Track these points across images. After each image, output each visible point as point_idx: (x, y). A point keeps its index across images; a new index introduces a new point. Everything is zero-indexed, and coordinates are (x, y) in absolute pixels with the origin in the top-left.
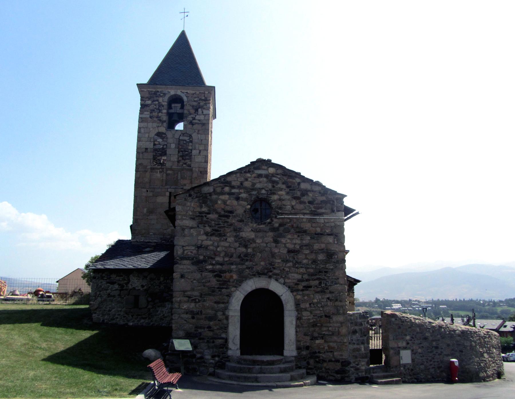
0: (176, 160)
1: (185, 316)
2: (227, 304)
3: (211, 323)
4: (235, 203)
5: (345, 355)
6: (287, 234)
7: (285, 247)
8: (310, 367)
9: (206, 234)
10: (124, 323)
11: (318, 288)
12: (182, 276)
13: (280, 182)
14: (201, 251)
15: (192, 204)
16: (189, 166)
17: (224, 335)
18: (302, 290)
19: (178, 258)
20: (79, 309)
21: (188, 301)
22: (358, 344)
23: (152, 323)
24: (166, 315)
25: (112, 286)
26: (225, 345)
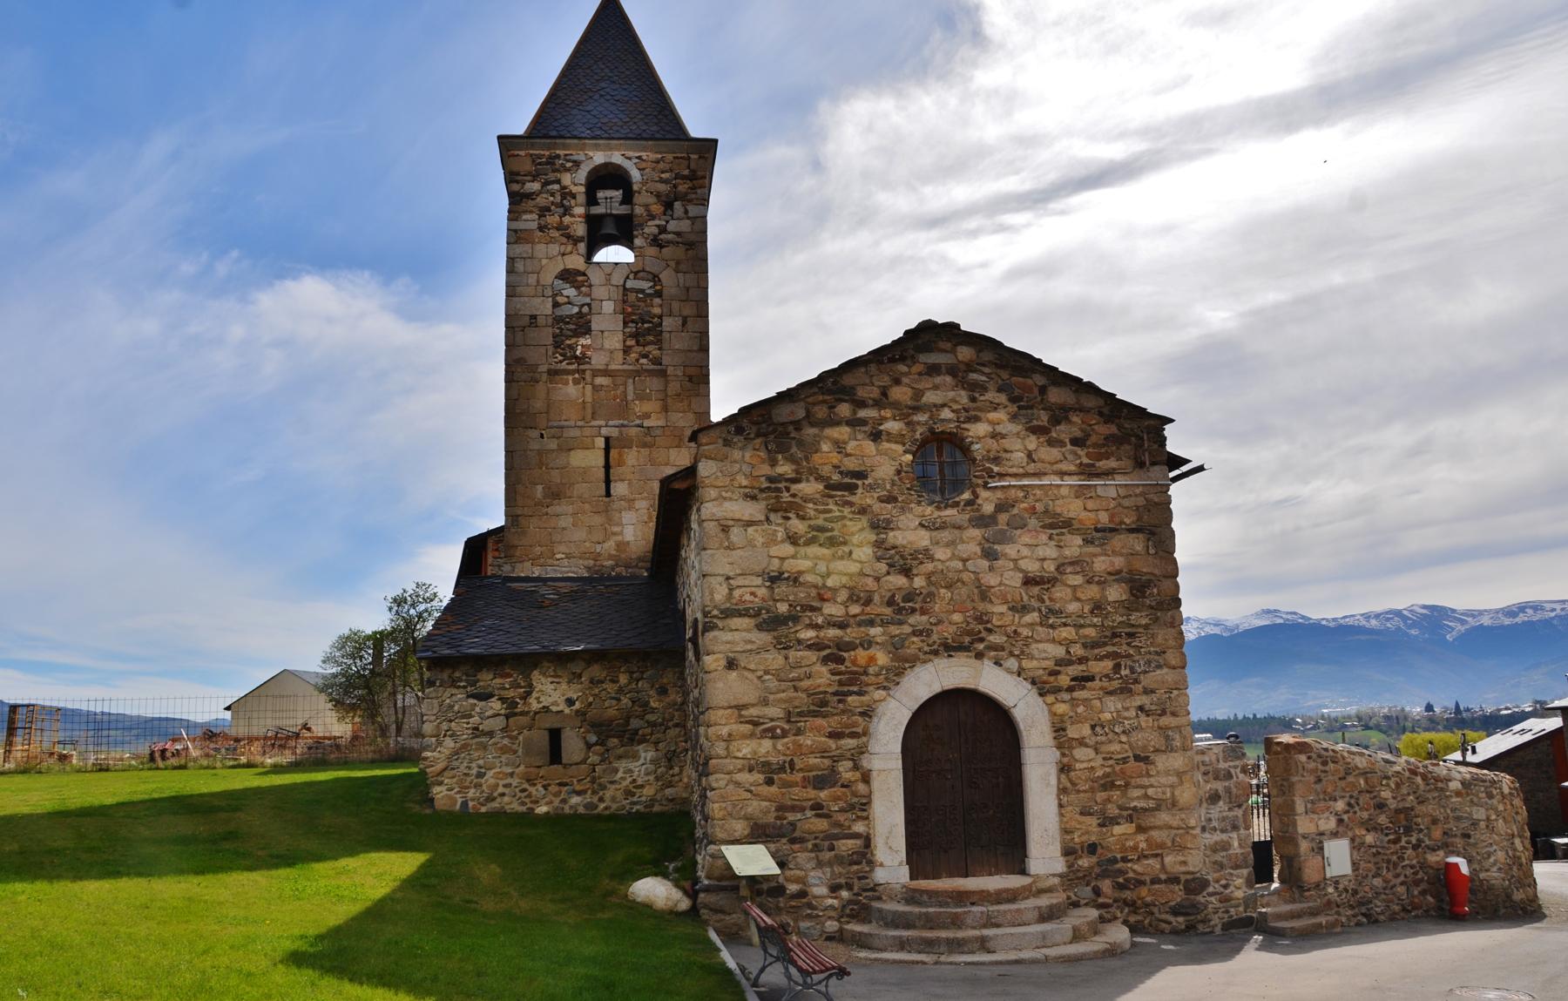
0: (619, 346)
1: (745, 777)
2: (864, 739)
3: (823, 794)
4: (870, 447)
5: (1196, 862)
6: (1018, 532)
7: (1017, 569)
8: (1101, 900)
9: (793, 539)
10: (524, 809)
11: (1111, 679)
12: (731, 665)
13: (991, 386)
14: (781, 589)
15: (747, 455)
16: (657, 361)
17: (859, 827)
18: (1070, 689)
19: (715, 612)
20: (350, 779)
21: (752, 736)
22: (1223, 831)
23: (602, 806)
24: (640, 782)
25: (483, 703)
26: (864, 854)
